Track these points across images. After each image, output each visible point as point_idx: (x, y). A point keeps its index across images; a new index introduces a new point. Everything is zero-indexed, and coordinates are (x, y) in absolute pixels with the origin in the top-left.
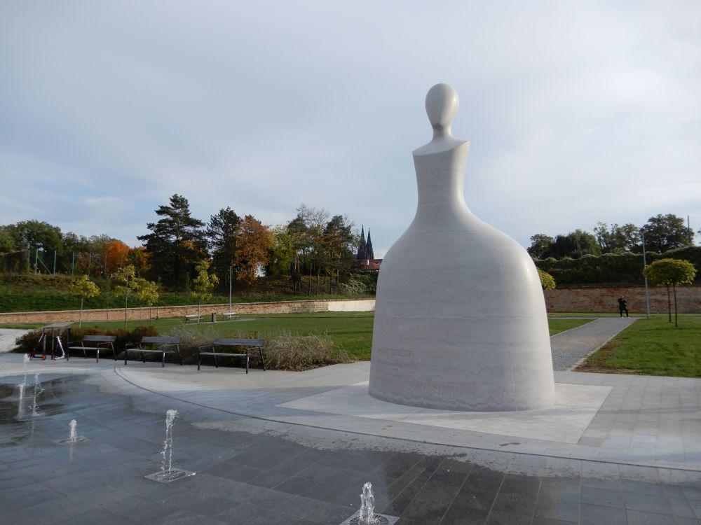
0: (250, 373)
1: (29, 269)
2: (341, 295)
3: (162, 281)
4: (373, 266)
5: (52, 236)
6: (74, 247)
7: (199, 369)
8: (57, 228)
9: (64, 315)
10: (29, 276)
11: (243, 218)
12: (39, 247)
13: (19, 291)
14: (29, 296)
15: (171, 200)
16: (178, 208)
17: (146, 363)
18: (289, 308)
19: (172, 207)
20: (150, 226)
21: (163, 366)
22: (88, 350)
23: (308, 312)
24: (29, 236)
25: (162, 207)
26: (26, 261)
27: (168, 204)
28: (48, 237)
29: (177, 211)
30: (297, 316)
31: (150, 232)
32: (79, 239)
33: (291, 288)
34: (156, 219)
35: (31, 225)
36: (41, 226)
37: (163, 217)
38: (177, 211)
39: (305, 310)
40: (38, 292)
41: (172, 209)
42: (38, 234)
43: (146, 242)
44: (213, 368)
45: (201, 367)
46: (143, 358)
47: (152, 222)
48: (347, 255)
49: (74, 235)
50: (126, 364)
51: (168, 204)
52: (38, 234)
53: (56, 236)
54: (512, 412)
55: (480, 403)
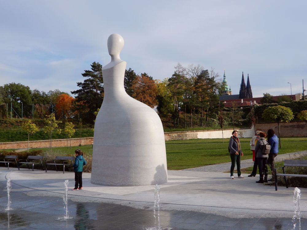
0: (65, 173)
1: (7, 115)
2: (209, 126)
3: (82, 122)
4: (246, 103)
5: (23, 91)
6: (38, 98)
7: (46, 172)
8: (28, 87)
9: (27, 144)
10: (8, 120)
11: (140, 75)
12: (18, 100)
13: (2, 129)
14: (7, 133)
15: (92, 66)
16: (97, 71)
17: (30, 169)
18: (169, 137)
19: (92, 71)
20: (79, 84)
21: (33, 171)
22: (58, 165)
23: (182, 140)
24: (12, 93)
25: (86, 71)
26: (6, 110)
27: (90, 69)
28: (22, 93)
29: (96, 73)
30: (174, 142)
31: (80, 88)
32: (41, 93)
33: (173, 123)
34: (82, 80)
35: (12, 85)
36: (18, 86)
37: (87, 78)
38: (96, 73)
39: (180, 138)
40: (12, 130)
41: (92, 72)
42: (16, 92)
43: (77, 95)
44: (55, 172)
45: (278, 187)
46: (29, 167)
47: (80, 82)
48: (213, 97)
49: (38, 91)
50: (19, 170)
51: (90, 69)
52: (16, 92)
53: (28, 93)
54: (132, 187)
55: (119, 183)
